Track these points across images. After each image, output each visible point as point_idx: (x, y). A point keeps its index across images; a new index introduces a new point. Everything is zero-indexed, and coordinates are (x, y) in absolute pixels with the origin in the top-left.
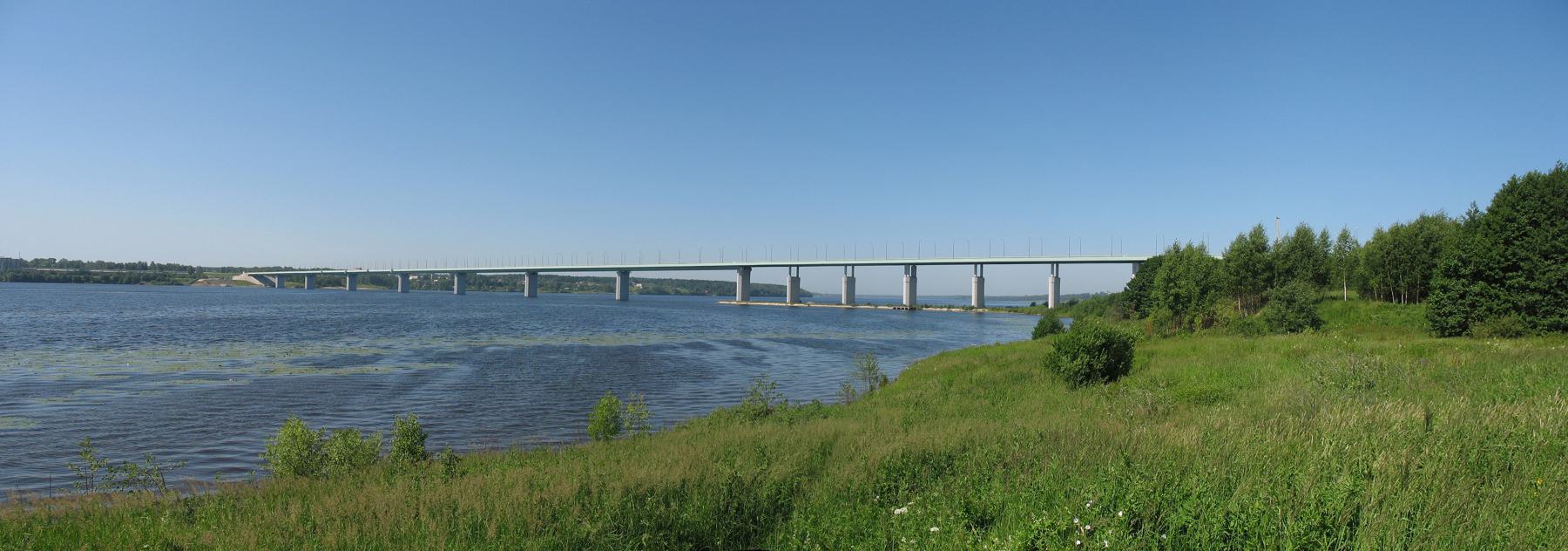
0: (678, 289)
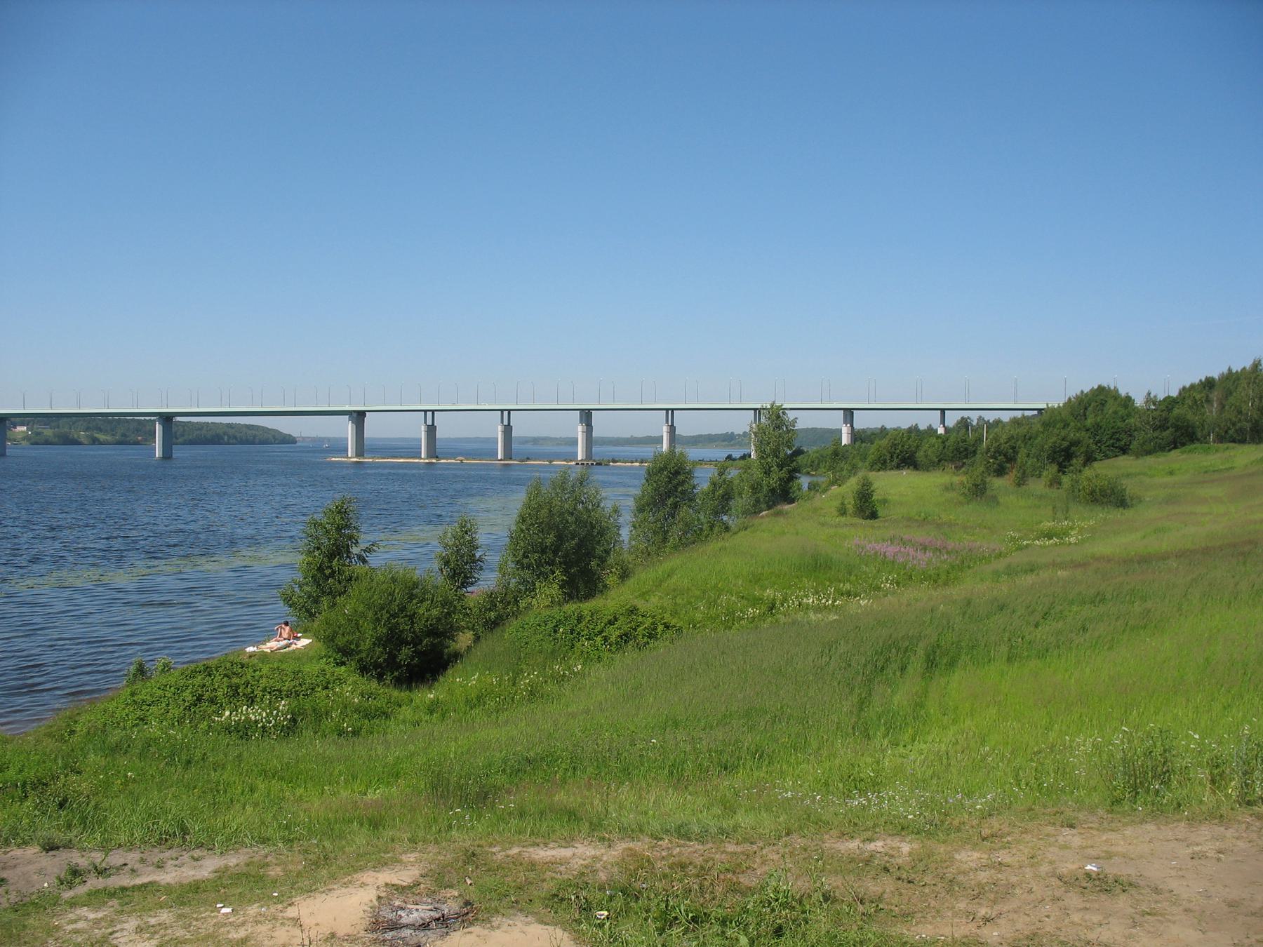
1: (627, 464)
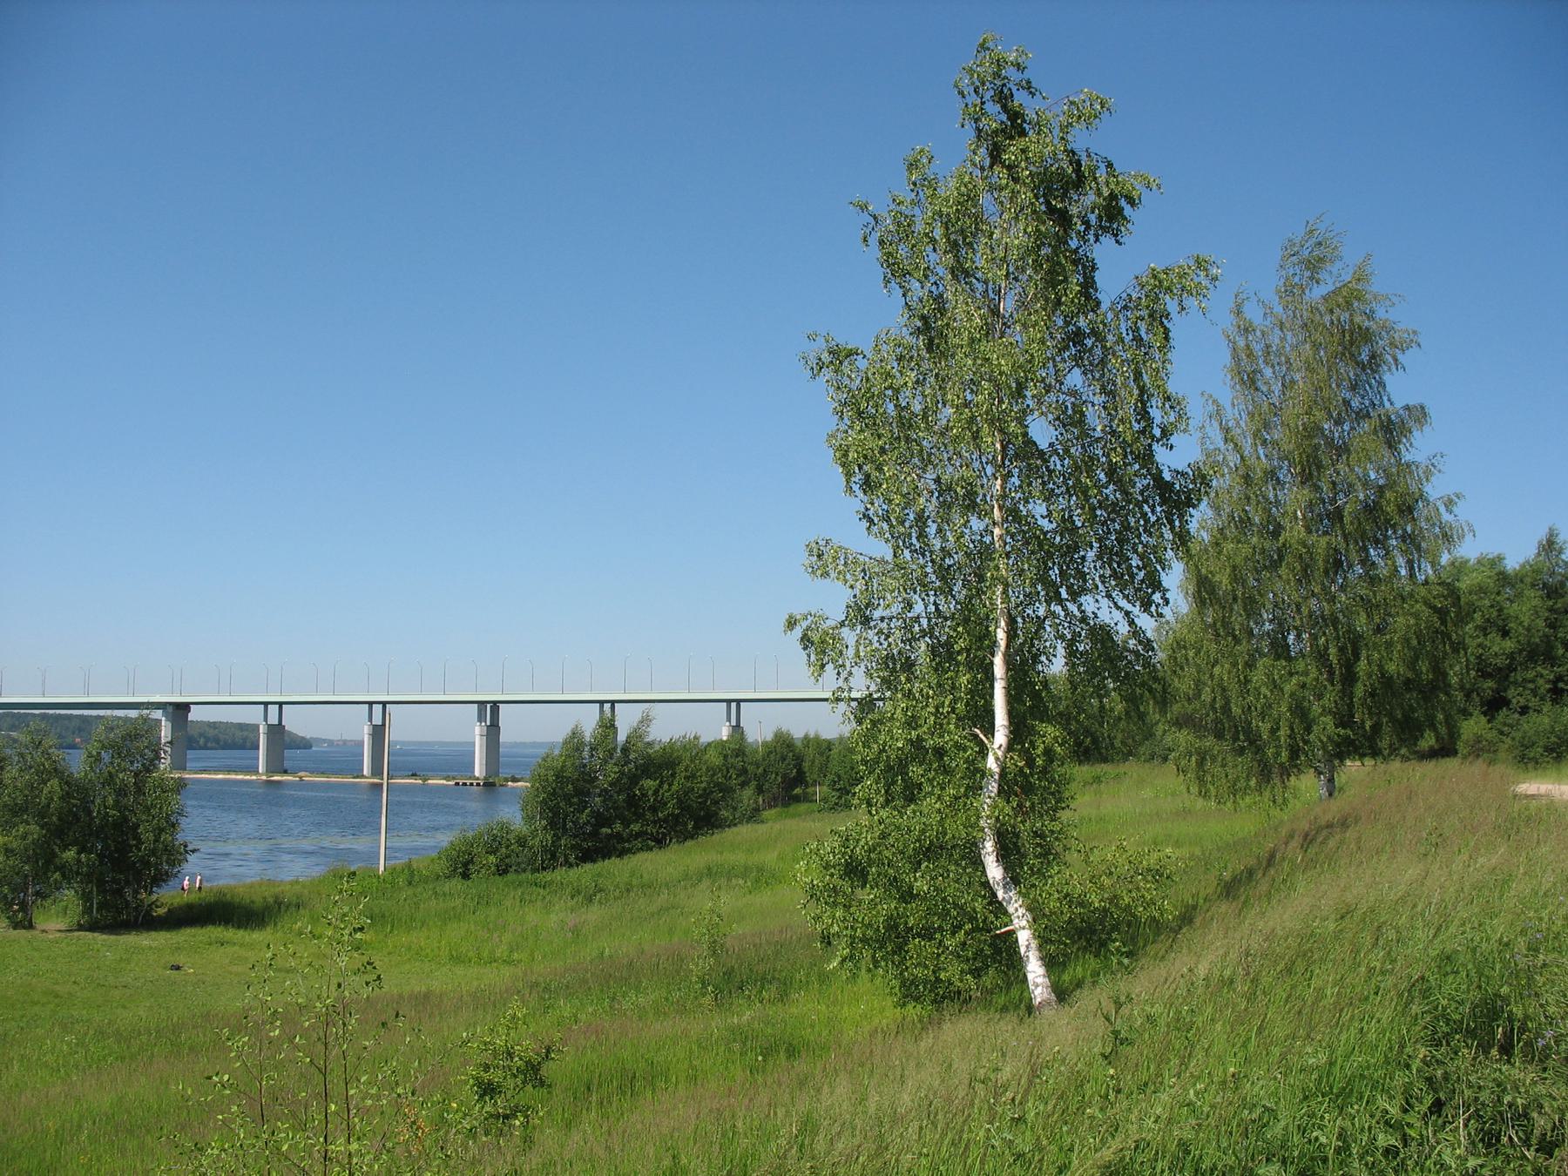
0: (14, 734)
1: (520, 784)
